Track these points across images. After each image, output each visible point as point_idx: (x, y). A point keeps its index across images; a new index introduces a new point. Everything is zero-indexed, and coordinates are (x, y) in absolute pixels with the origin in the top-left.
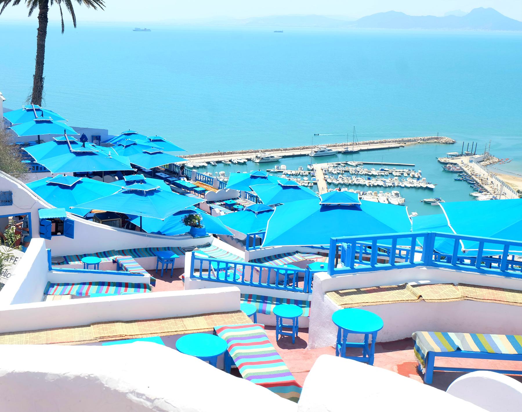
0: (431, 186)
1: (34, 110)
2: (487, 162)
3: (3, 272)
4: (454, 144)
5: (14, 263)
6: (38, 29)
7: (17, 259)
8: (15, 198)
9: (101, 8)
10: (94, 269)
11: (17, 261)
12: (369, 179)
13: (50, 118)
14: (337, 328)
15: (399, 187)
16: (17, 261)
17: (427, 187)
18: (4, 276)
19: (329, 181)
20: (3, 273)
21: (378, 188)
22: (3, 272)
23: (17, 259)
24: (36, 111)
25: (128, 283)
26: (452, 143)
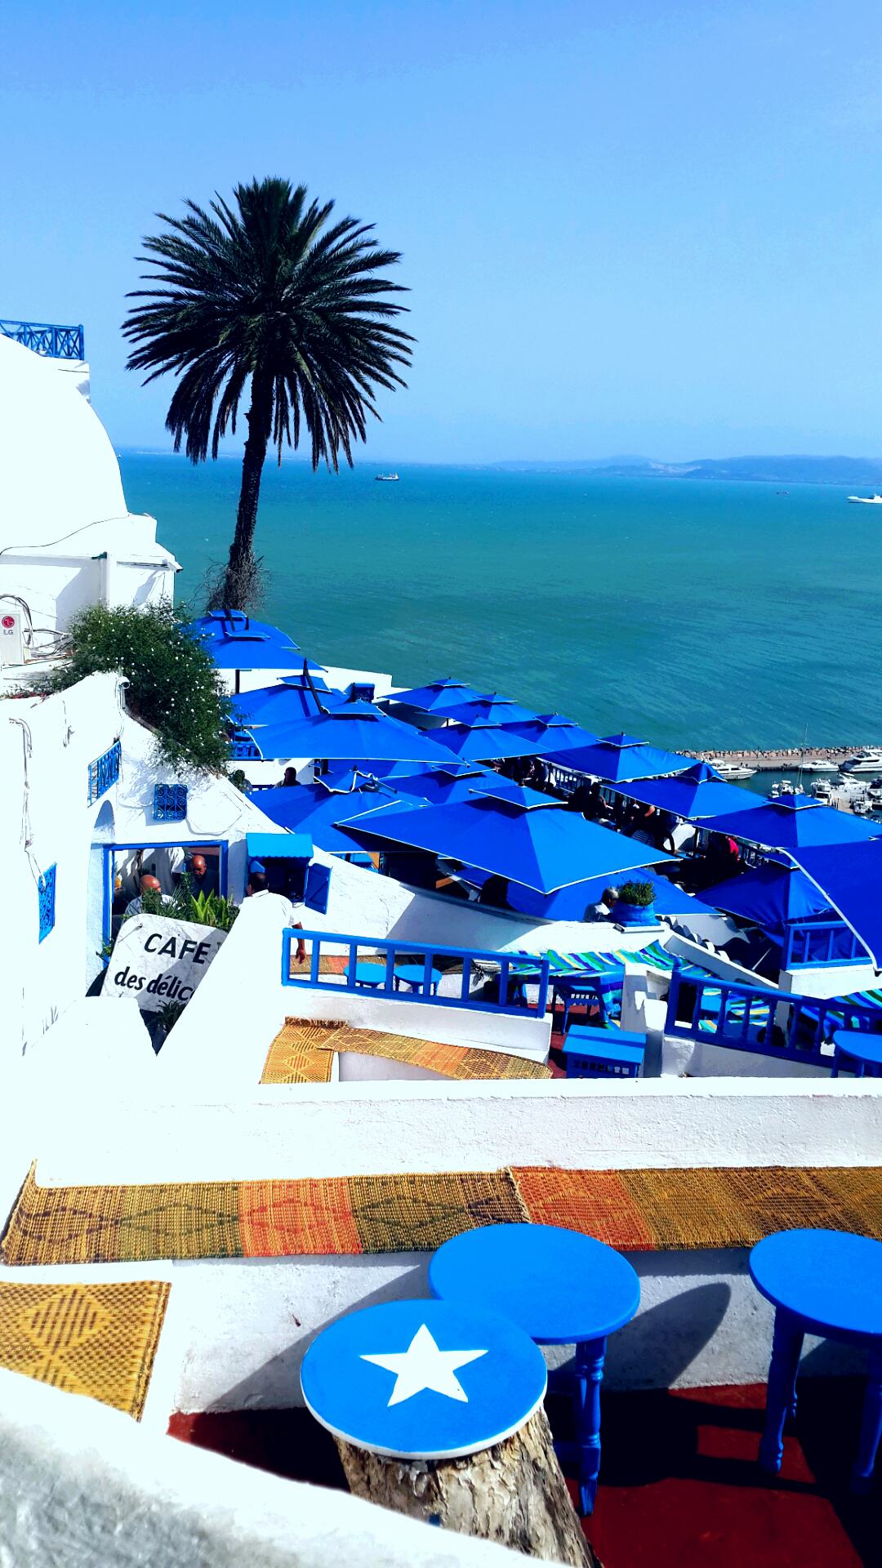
7: (205, 949)
16: (206, 953)
23: (205, 949)
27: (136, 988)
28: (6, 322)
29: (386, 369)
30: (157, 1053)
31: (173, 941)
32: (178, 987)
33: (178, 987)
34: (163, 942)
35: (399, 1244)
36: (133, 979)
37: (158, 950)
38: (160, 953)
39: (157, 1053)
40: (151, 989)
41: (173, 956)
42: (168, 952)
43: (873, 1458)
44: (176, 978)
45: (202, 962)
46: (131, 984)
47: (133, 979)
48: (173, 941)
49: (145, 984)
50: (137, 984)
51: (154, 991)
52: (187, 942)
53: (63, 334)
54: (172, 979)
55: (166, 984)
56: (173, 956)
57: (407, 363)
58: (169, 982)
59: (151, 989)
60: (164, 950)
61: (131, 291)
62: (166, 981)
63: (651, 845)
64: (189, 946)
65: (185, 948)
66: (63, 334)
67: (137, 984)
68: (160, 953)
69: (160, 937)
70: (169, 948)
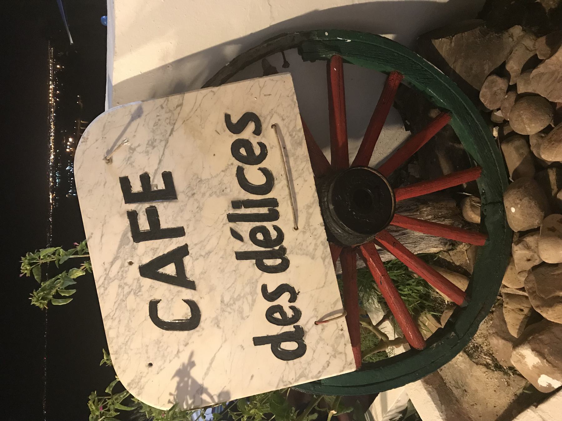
7: (137, 187)
23: (137, 187)
27: (293, 299)
36: (277, 315)
38: (191, 285)
41: (183, 251)
42: (180, 268)
45: (167, 177)
50: (284, 300)
56: (183, 251)
58: (245, 228)
70: (170, 269)
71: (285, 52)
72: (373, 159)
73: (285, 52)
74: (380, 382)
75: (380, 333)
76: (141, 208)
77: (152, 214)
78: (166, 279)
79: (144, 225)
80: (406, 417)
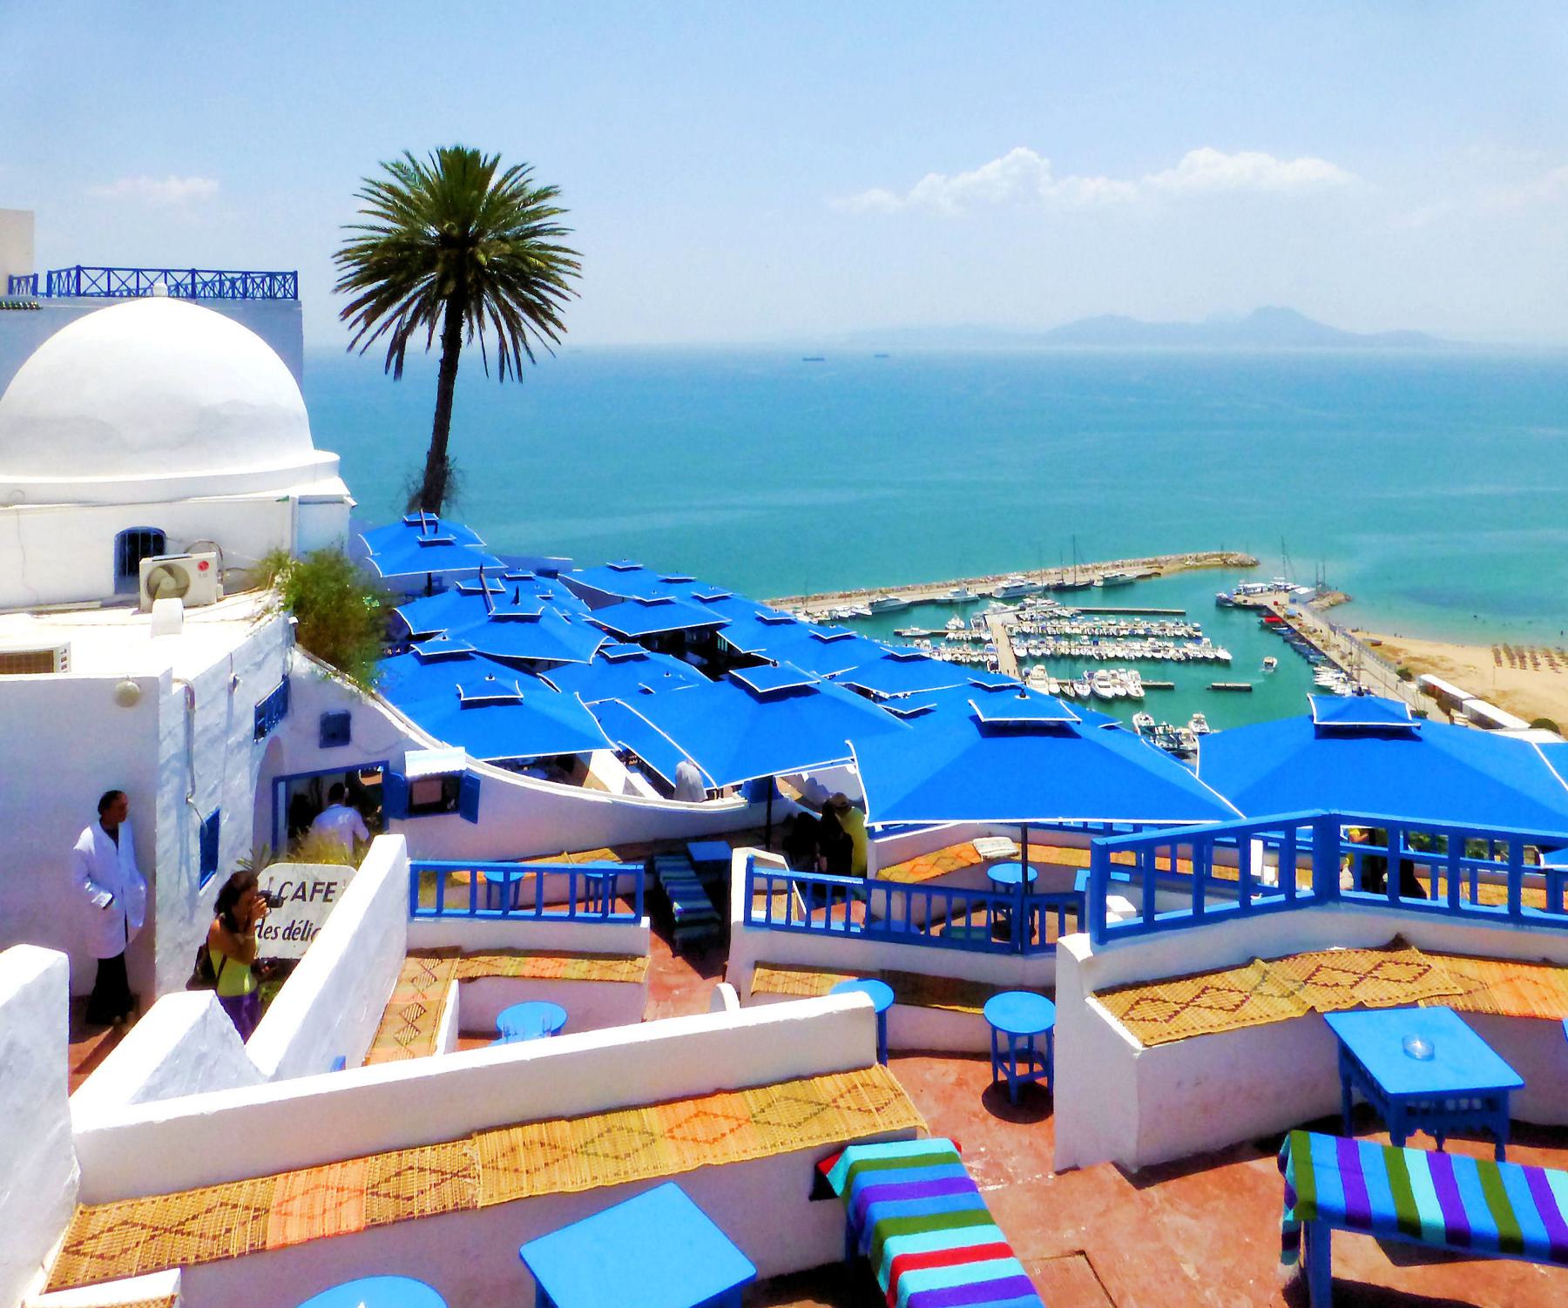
0: (1224, 654)
1: (424, 523)
2: (1325, 602)
3: (297, 931)
4: (1257, 567)
5: (326, 899)
6: (441, 361)
7: (332, 888)
8: (356, 729)
9: (98, 267)
10: (583, 909)
11: (333, 892)
12: (1096, 643)
13: (452, 538)
14: (991, 1027)
15: (1191, 663)
16: (333, 892)
17: (1153, 657)
18: (302, 939)
19: (1022, 653)
20: (299, 933)
21: (1118, 664)
22: (297, 931)
23: (332, 888)
24: (427, 525)
25: (1055, 951)
26: (1251, 565)
27: (272, 938)
28: (227, 272)
29: (560, 283)
30: (1053, 1001)
31: (303, 885)
32: (310, 929)
33: (310, 929)
34: (296, 885)
35: (372, 1221)
36: (269, 930)
37: (290, 897)
38: (292, 900)
39: (1053, 1001)
40: (286, 936)
41: (304, 900)
42: (298, 897)
43: (608, 740)
44: (308, 921)
45: (331, 901)
46: (267, 935)
47: (269, 930)
48: (303, 885)
49: (280, 932)
50: (273, 934)
51: (288, 938)
52: (316, 884)
53: (280, 278)
54: (305, 923)
55: (299, 928)
56: (304, 900)
57: (578, 276)
58: (302, 926)
59: (286, 936)
60: (295, 896)
61: (347, 238)
62: (299, 926)
63: (726, 956)
64: (318, 887)
65: (314, 890)
66: (280, 278)
67: (273, 934)
68: (292, 900)
69: (291, 884)
70: (300, 893)
71: (991, 889)
72: (1405, 1285)
73: (991, 889)
74: (579, 852)
75: (492, 1127)
76: (324, 888)
77: (320, 891)
78: (297, 892)
79: (318, 887)
80: (88, 1043)
